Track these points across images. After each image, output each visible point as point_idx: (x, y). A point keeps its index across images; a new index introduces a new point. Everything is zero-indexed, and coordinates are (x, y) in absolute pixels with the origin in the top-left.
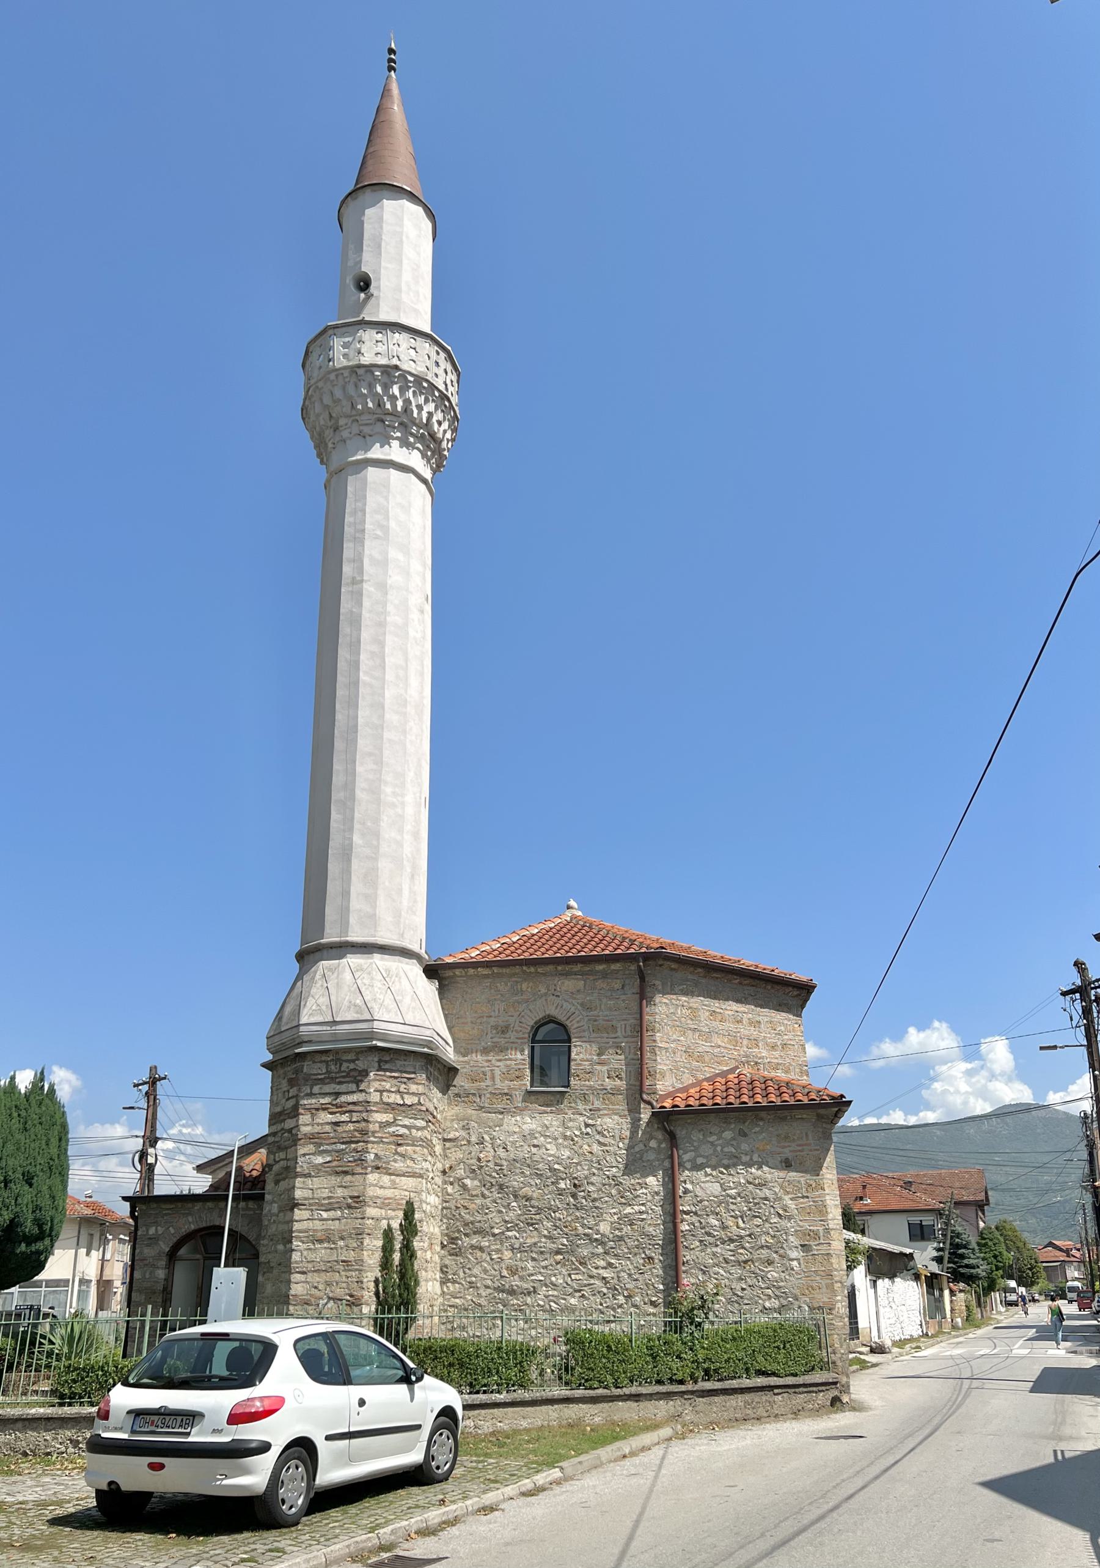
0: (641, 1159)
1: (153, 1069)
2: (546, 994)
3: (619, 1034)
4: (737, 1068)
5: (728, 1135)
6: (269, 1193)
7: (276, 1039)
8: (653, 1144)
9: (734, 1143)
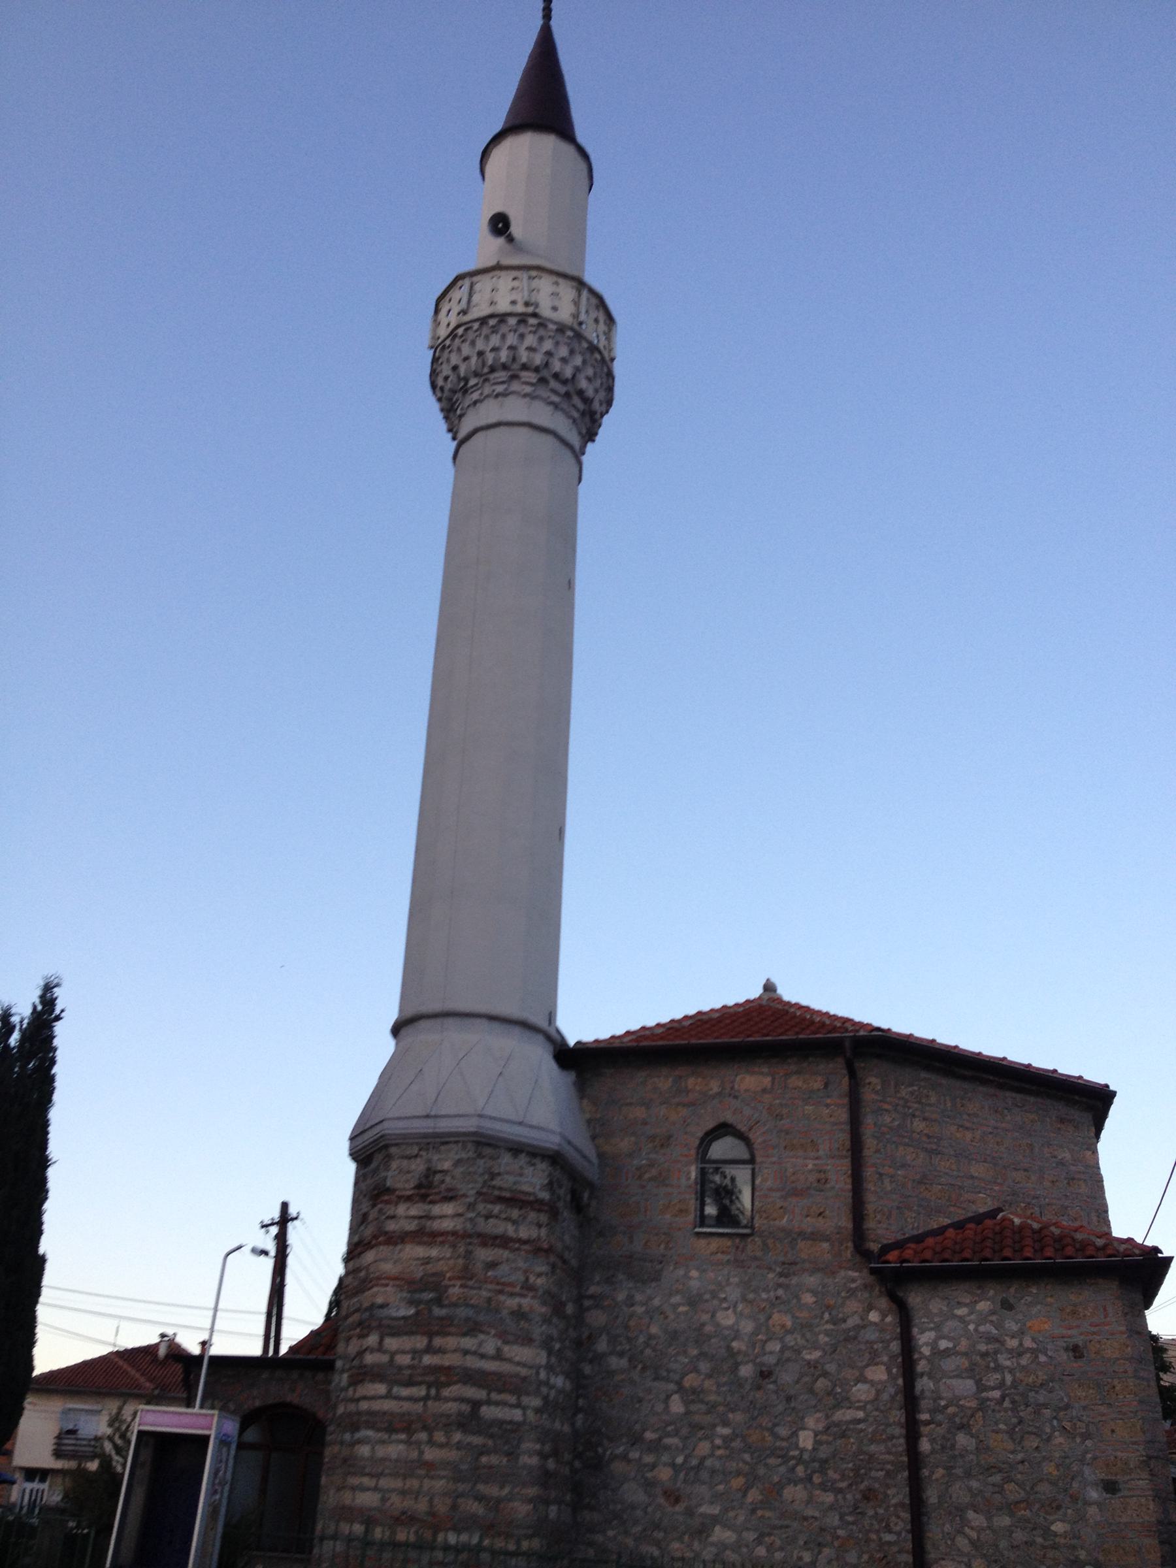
0: (855, 1338)
1: (285, 1206)
2: (719, 1094)
3: (821, 1153)
4: (1000, 1210)
5: (984, 1306)
6: (340, 1357)
7: (360, 1140)
8: (874, 1316)
9: (994, 1318)
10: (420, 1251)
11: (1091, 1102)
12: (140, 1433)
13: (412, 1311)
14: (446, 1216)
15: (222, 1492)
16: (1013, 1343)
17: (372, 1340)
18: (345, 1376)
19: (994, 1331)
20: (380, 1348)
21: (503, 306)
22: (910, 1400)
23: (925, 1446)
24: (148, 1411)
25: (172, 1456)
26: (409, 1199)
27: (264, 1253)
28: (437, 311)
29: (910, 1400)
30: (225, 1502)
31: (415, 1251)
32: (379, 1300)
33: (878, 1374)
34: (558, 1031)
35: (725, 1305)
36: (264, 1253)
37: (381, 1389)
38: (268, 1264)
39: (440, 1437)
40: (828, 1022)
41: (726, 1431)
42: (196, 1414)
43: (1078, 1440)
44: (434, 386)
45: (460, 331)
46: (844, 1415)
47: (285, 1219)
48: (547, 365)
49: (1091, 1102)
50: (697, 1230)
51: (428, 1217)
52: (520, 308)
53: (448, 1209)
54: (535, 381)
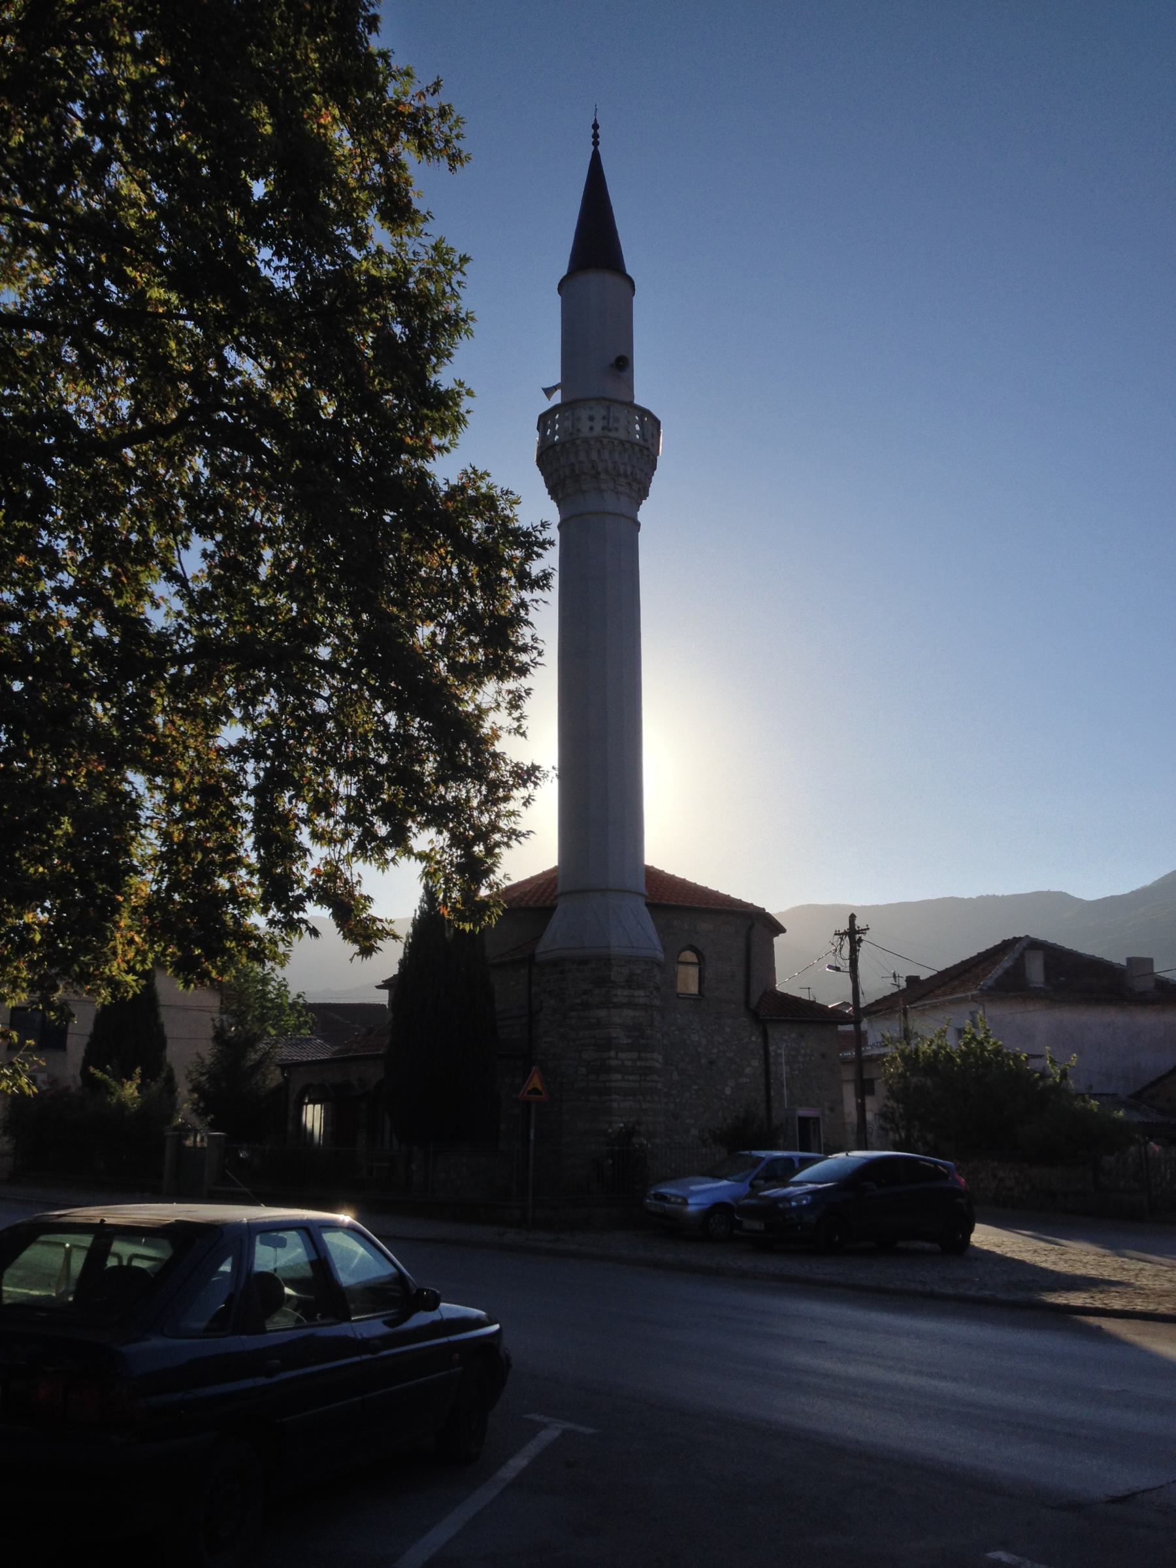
5: (793, 1035)
8: (754, 1038)
10: (631, 1013)
14: (640, 995)
16: (803, 1052)
17: (613, 1054)
20: (617, 1058)
22: (767, 1072)
23: (772, 1093)
26: (622, 987)
29: (767, 1072)
31: (629, 1013)
32: (614, 1035)
33: (755, 1063)
37: (619, 1076)
39: (648, 1098)
41: (696, 1087)
46: (744, 1080)
51: (633, 996)
53: (642, 993)
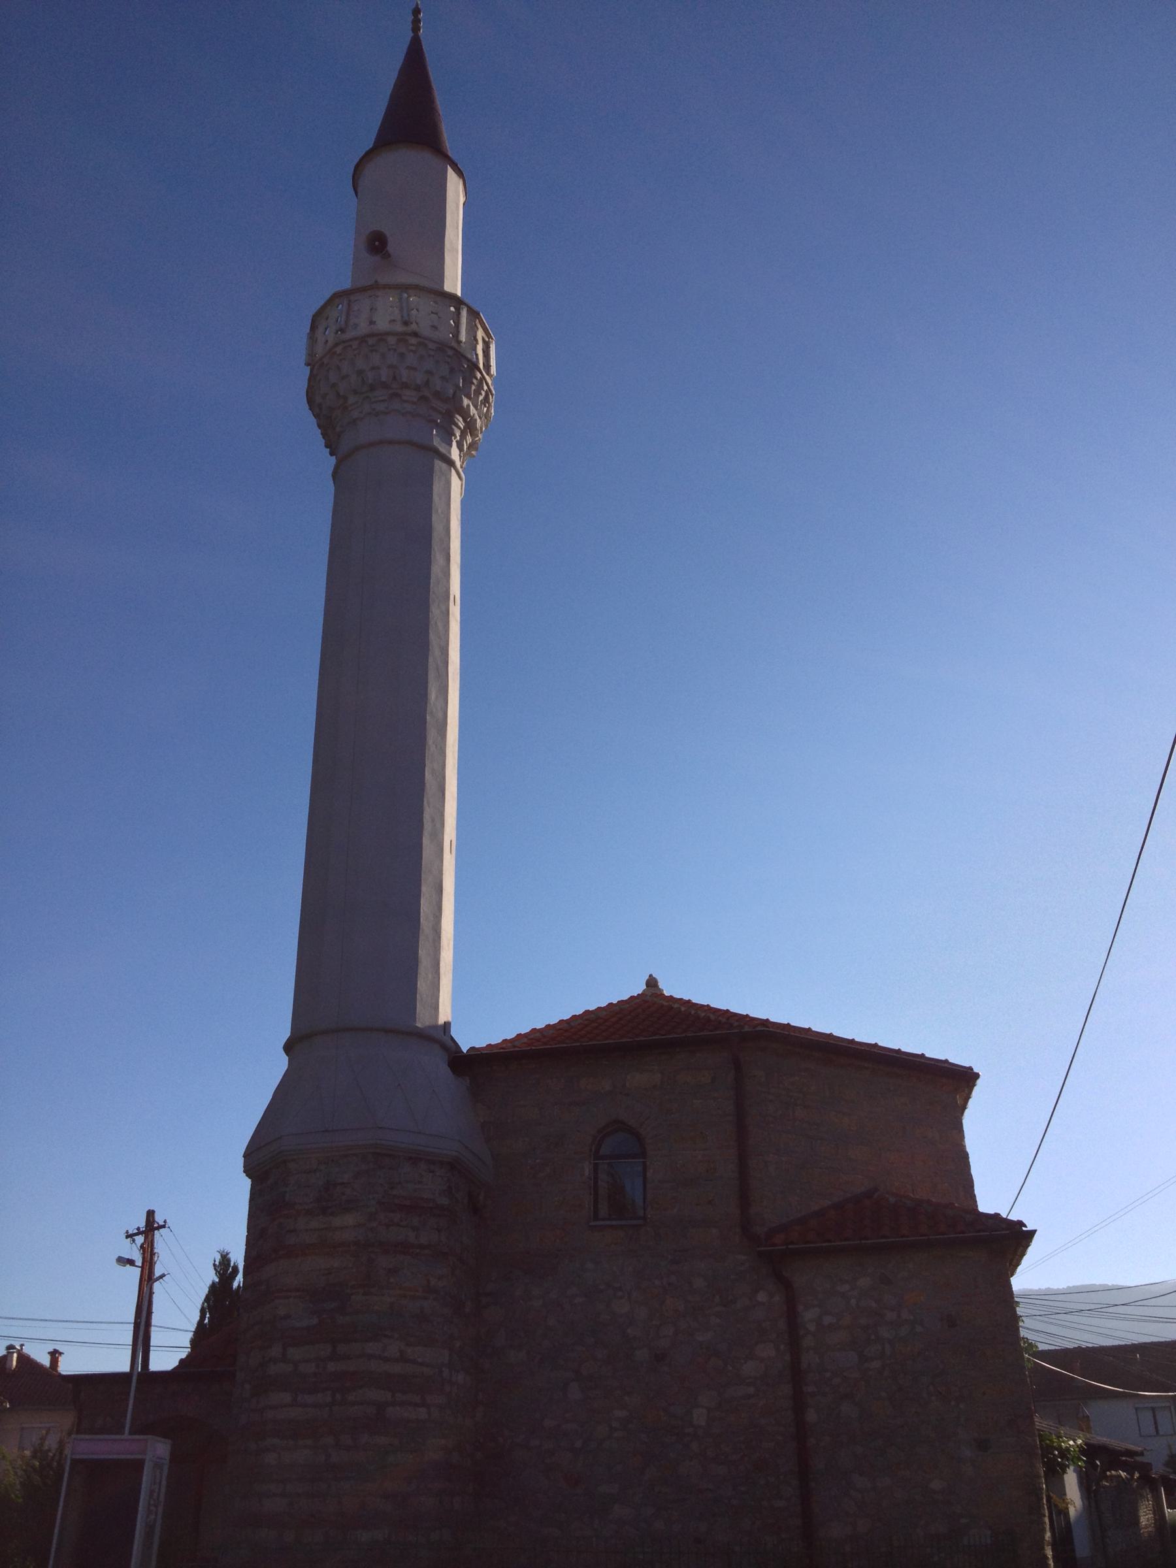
1: (150, 1214)
8: (762, 1297)
11: (957, 1081)
12: (72, 1460)
13: (315, 1321)
15: (156, 1514)
18: (247, 1386)
19: (874, 1305)
21: (382, 325)
23: (811, 1416)
24: (82, 1440)
25: (111, 1482)
27: (131, 1262)
28: (313, 328)
30: (159, 1522)
34: (452, 1039)
35: (620, 1294)
36: (131, 1262)
37: (287, 1397)
38: (134, 1273)
40: (712, 1017)
42: (127, 1440)
43: (953, 1403)
44: (310, 401)
45: (339, 350)
47: (151, 1226)
48: (427, 383)
49: (957, 1081)
50: (592, 1224)
52: (399, 328)
53: (349, 1219)
54: (415, 400)
